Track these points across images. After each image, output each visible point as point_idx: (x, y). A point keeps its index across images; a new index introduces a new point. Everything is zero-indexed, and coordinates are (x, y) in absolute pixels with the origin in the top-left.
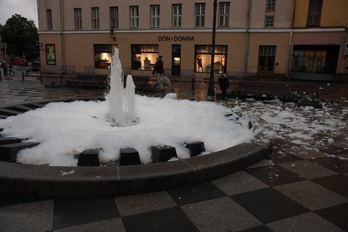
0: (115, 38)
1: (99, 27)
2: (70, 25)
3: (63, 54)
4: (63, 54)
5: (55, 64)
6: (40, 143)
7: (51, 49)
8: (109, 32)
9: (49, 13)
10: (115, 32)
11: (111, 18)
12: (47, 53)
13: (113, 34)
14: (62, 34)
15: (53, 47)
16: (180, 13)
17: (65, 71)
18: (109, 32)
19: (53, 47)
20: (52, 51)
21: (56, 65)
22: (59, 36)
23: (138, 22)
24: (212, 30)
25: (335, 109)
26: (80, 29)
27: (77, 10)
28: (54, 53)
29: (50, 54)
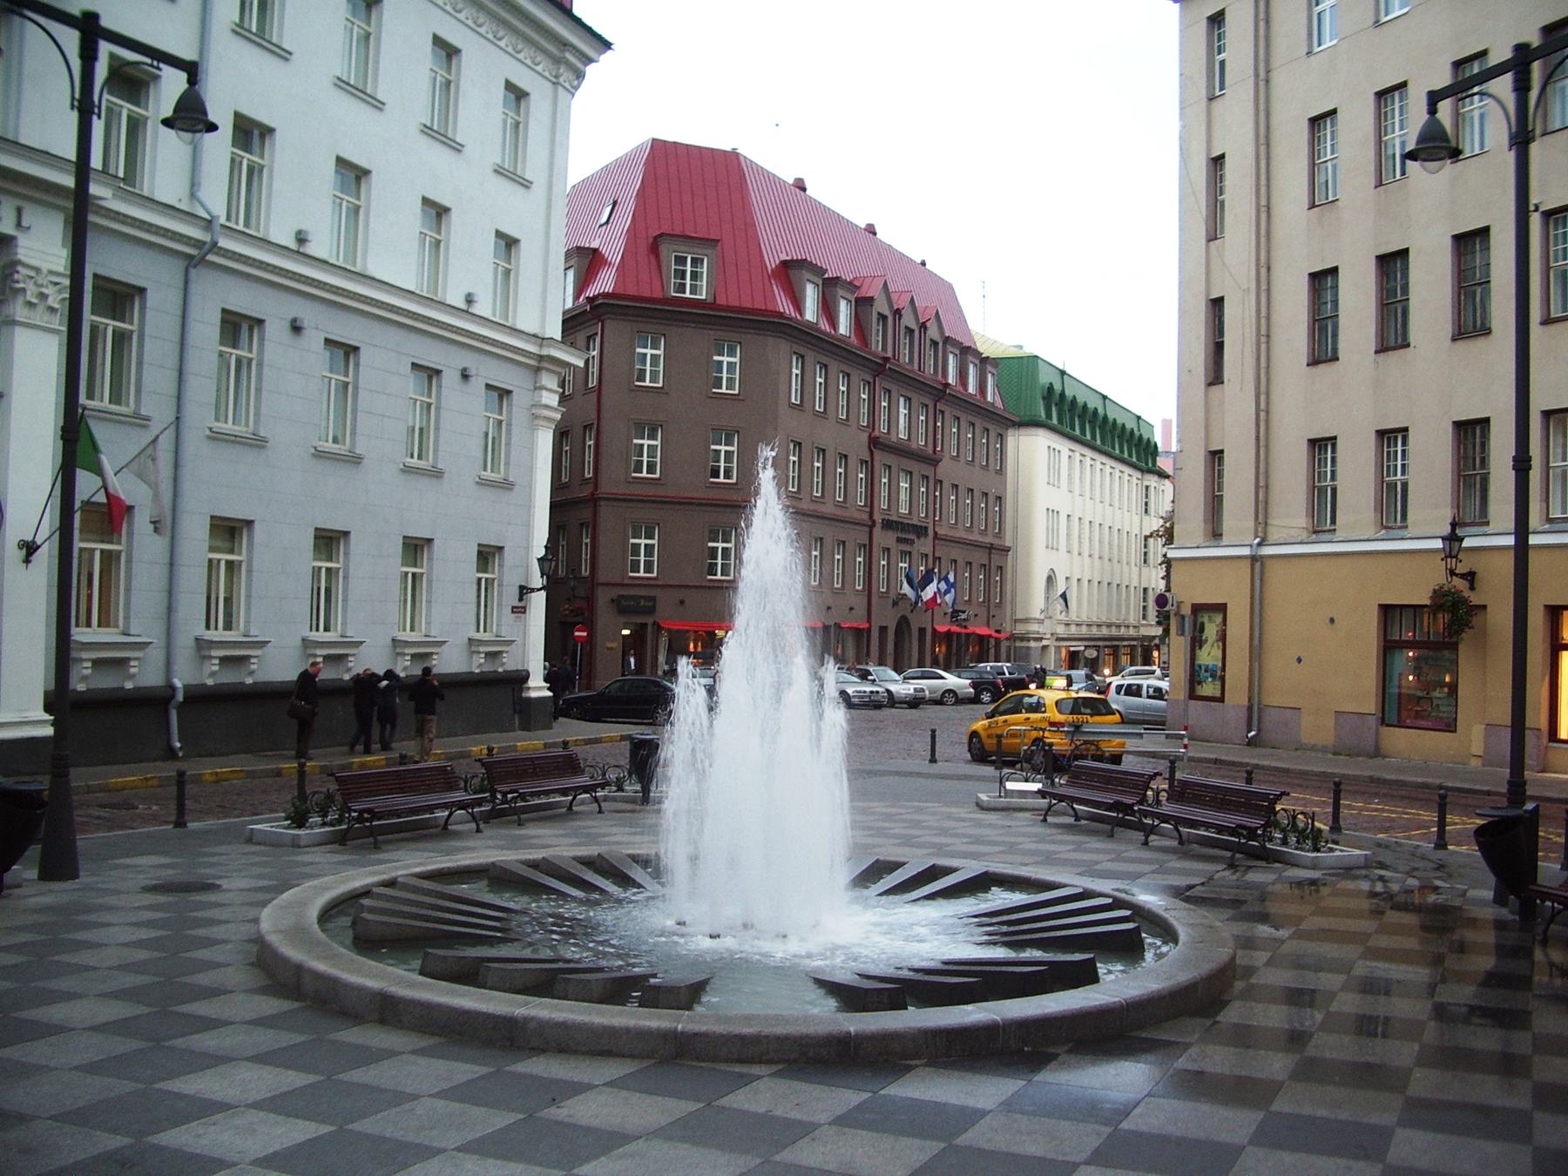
0: (1474, 573)
1: (1333, 521)
2: (1291, 511)
3: (1257, 651)
4: (1257, 651)
5: (1221, 699)
6: (815, 979)
7: (1211, 631)
8: (1438, 544)
9: (1389, 447)
10: (1467, 543)
11: (1459, 476)
12: (1197, 644)
13: (1456, 557)
14: (1254, 559)
15: (1219, 618)
16: (1404, 444)
17: (1259, 731)
18: (1438, 544)
19: (1219, 618)
20: (1214, 637)
21: (1223, 702)
22: (1247, 565)
23: (1407, 490)
24: (1531, 542)
25: (601, 948)
26: (1400, 528)
27: (1321, 446)
28: (1221, 644)
29: (1206, 648)
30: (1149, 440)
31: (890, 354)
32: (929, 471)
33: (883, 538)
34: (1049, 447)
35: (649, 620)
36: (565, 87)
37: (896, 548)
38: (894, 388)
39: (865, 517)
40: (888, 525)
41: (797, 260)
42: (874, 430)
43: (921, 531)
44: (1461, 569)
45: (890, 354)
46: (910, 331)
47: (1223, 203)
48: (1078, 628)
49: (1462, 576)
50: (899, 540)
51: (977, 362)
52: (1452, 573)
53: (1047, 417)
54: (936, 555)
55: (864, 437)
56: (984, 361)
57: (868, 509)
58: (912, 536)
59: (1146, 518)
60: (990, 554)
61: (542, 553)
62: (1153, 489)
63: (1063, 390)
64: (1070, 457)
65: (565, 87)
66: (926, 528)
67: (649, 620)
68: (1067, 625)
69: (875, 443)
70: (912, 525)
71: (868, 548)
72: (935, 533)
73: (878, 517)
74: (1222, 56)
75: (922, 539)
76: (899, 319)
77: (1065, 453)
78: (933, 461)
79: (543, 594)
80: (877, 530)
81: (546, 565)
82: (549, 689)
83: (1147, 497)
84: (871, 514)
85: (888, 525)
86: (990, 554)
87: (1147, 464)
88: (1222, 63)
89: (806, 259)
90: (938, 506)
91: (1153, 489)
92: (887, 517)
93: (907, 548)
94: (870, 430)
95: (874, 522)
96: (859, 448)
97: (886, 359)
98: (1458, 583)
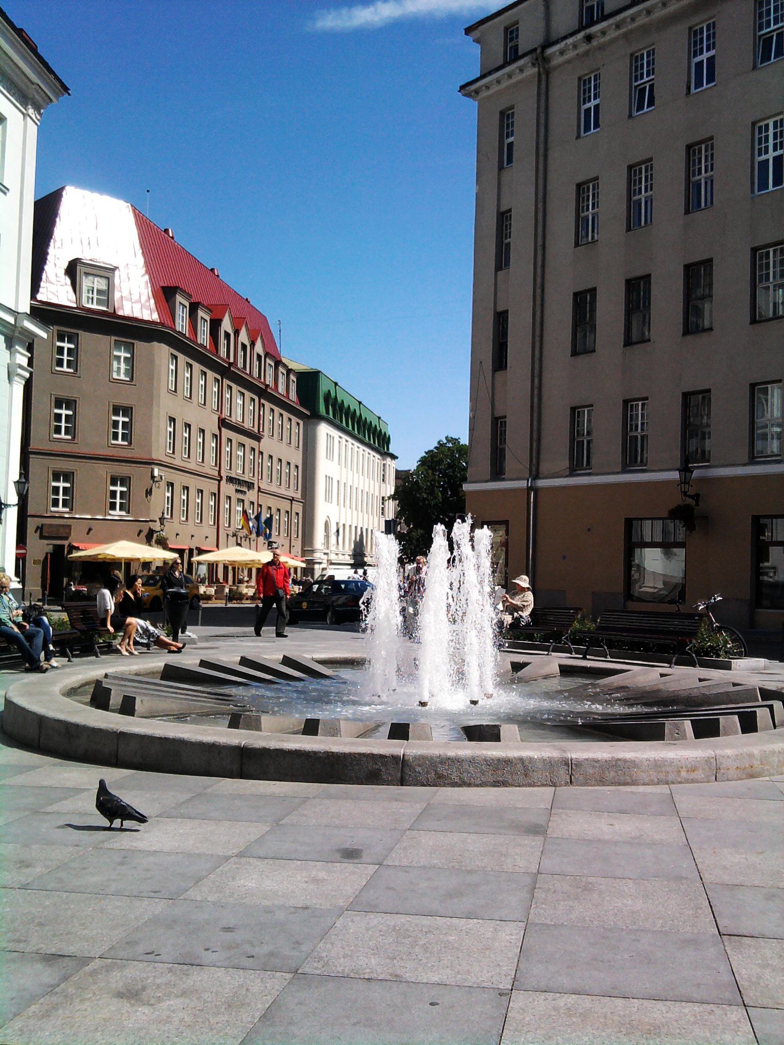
8: (675, 475)
13: (688, 483)
28: (504, 549)
30: (385, 433)
31: (232, 360)
32: (254, 444)
33: (228, 489)
34: (327, 434)
35: (66, 543)
36: (31, 118)
37: (235, 496)
38: (234, 386)
39: (216, 473)
40: (231, 480)
41: (171, 287)
42: (221, 413)
43: (250, 485)
44: (691, 492)
45: (232, 360)
46: (244, 347)
47: (508, 245)
48: (343, 556)
49: (691, 497)
50: (237, 491)
51: (285, 372)
52: (685, 494)
53: (326, 414)
54: (260, 503)
55: (216, 418)
56: (289, 371)
57: (218, 469)
58: (245, 489)
59: (383, 485)
60: (291, 503)
61: (17, 478)
62: (388, 466)
63: (336, 396)
64: (339, 442)
65: (31, 118)
66: (253, 484)
67: (66, 543)
68: (337, 554)
69: (223, 423)
70: (245, 481)
71: (216, 496)
72: (259, 488)
73: (223, 474)
74: (511, 139)
75: (251, 491)
76: (238, 337)
77: (337, 439)
78: (257, 438)
79: (16, 508)
80: (223, 482)
81: (21, 485)
82: (19, 582)
83: (384, 470)
84: (219, 472)
85: (231, 480)
86: (291, 503)
87: (384, 449)
88: (510, 145)
89: (179, 287)
90: (260, 470)
91: (388, 466)
92: (229, 475)
93: (241, 496)
94: (219, 413)
95: (221, 477)
96: (212, 426)
97: (230, 364)
98: (690, 501)
